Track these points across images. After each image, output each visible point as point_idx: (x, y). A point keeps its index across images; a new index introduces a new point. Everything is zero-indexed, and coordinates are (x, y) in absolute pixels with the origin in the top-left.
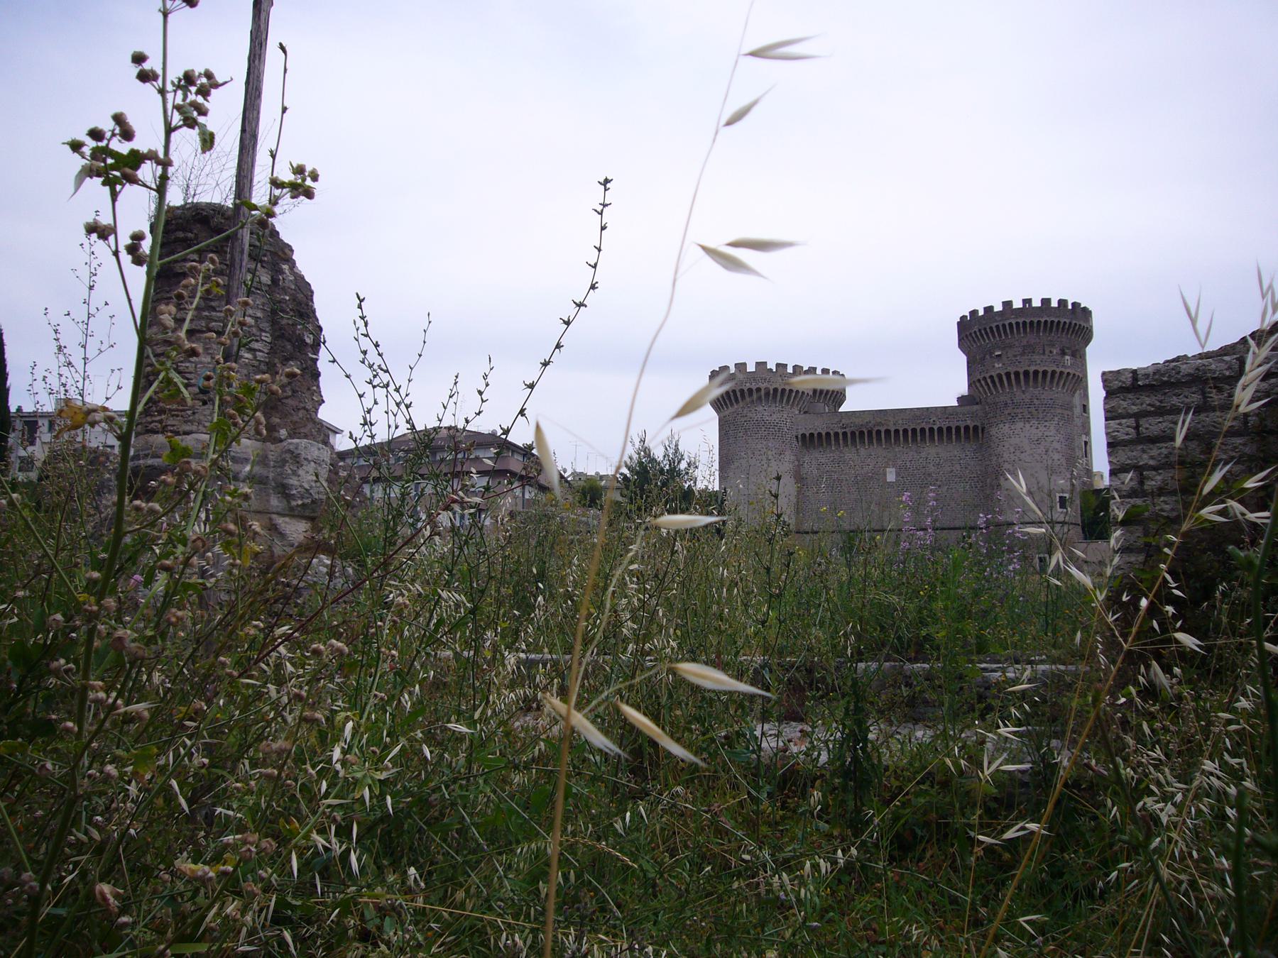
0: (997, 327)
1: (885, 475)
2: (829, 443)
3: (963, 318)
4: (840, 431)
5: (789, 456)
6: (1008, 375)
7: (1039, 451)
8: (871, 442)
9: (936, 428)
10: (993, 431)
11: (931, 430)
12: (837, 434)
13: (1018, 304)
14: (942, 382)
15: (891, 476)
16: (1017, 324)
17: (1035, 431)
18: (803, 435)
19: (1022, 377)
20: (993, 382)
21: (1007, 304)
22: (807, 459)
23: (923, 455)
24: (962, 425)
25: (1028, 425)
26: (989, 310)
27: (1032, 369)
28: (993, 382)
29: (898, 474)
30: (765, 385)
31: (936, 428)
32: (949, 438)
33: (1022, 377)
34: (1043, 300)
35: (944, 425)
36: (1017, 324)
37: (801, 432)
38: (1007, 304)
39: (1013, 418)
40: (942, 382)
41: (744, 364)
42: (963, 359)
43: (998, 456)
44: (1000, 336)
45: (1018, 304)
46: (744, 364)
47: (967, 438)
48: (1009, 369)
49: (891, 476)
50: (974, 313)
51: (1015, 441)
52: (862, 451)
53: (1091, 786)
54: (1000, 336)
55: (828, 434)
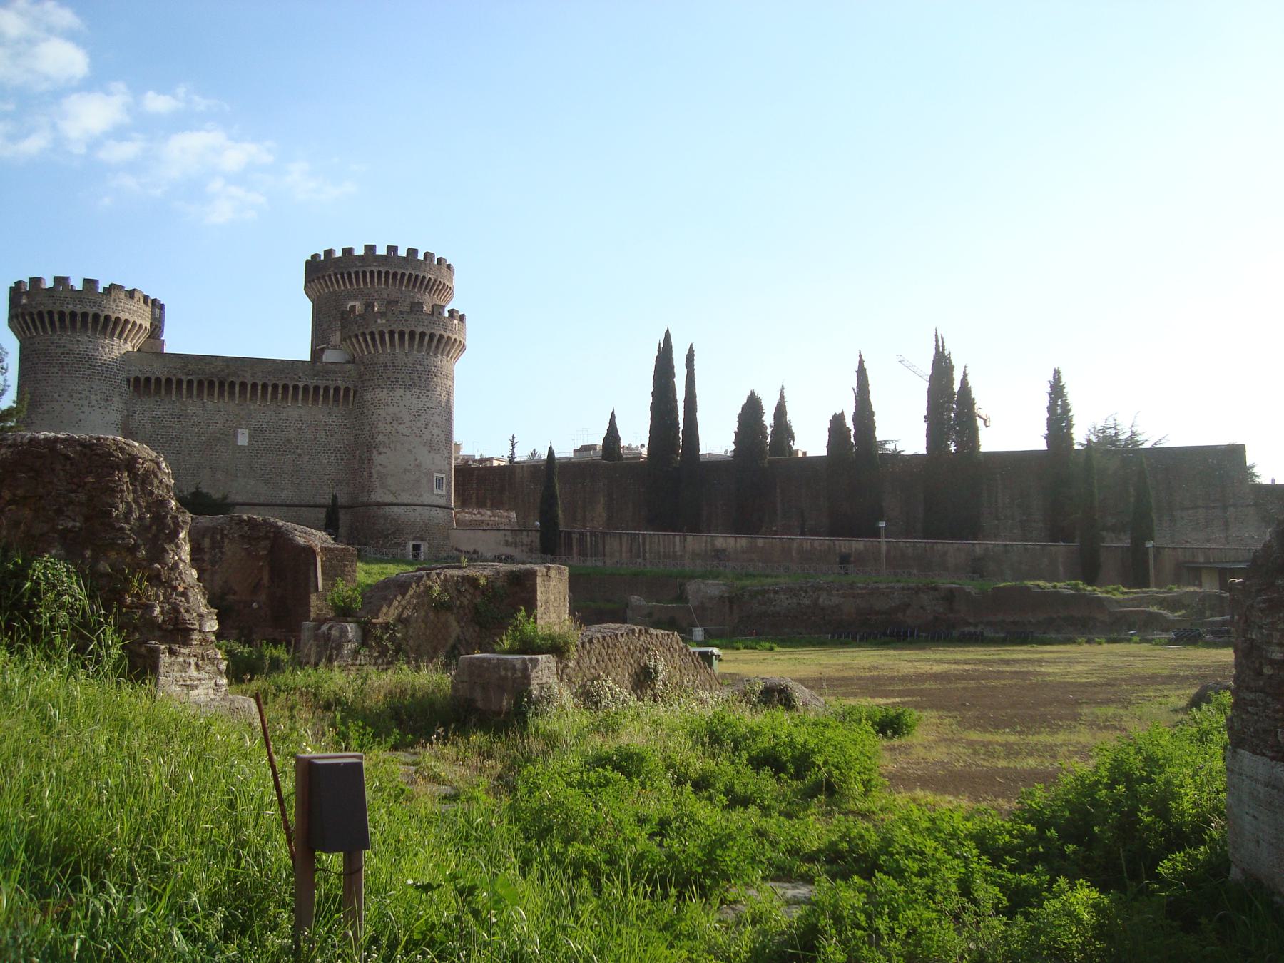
0: (403, 275)
1: (235, 436)
2: (168, 391)
3: (315, 256)
4: (185, 378)
5: (117, 403)
6: (392, 333)
7: (419, 424)
8: (316, 400)
9: (301, 385)
10: (368, 396)
11: (296, 388)
12: (180, 382)
13: (381, 251)
14: (282, 330)
15: (243, 439)
16: (410, 275)
17: (415, 400)
18: (137, 379)
19: (407, 337)
20: (373, 339)
21: (370, 249)
22: (138, 409)
23: (283, 416)
24: (332, 385)
25: (408, 393)
26: (348, 251)
27: (419, 330)
28: (373, 339)
29: (251, 437)
30: (95, 310)
31: (301, 385)
32: (316, 400)
33: (407, 337)
34: (409, 250)
35: (312, 383)
36: (380, 273)
37: (133, 375)
38: (370, 249)
39: (392, 384)
40: (282, 330)
41: (374, 247)
42: (308, 306)
43: (373, 425)
44: (358, 284)
45: (381, 251)
46: (374, 247)
47: (336, 400)
48: (394, 327)
49: (243, 439)
50: (36, 282)
51: (391, 409)
52: (210, 405)
53: (843, 943)
54: (358, 284)
55: (169, 381)
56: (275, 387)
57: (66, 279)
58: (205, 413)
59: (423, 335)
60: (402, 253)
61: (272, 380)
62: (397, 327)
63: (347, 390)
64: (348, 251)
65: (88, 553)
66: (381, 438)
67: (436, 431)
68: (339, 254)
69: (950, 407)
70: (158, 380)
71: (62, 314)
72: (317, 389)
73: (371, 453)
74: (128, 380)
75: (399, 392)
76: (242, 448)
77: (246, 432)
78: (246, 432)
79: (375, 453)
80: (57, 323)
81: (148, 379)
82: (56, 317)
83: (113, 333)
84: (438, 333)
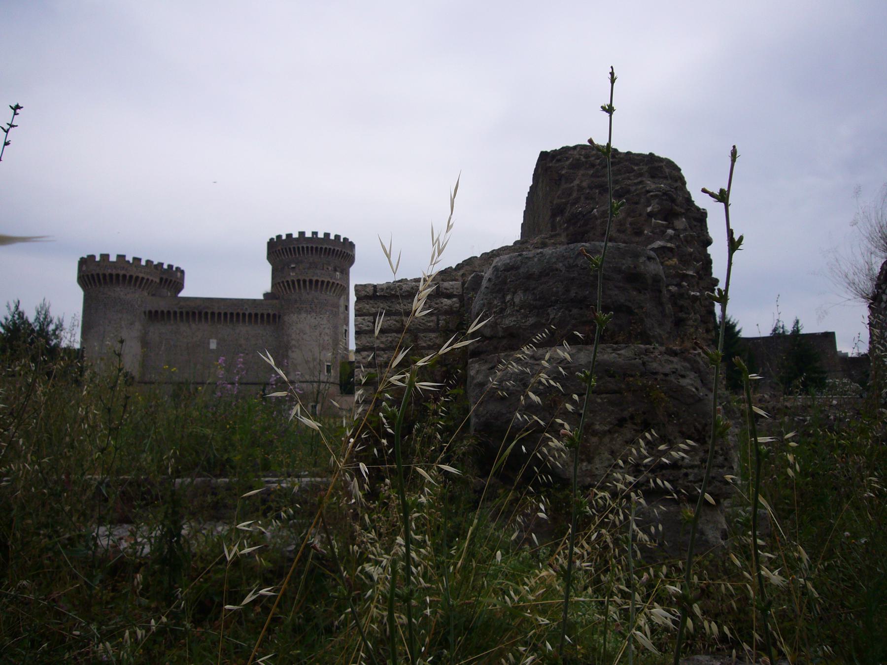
1: (209, 344)
3: (272, 239)
5: (138, 326)
6: (299, 281)
8: (256, 322)
9: (247, 313)
10: (286, 318)
13: (308, 235)
14: (254, 282)
17: (313, 320)
18: (150, 312)
19: (308, 283)
20: (288, 285)
21: (302, 234)
27: (314, 279)
28: (288, 285)
29: (218, 344)
31: (247, 313)
35: (253, 312)
37: (148, 309)
38: (302, 234)
40: (254, 282)
45: (308, 235)
49: (213, 345)
52: (194, 326)
55: (169, 312)
56: (232, 314)
57: (124, 256)
58: (190, 332)
59: (317, 281)
60: (332, 237)
61: (229, 311)
62: (301, 278)
63: (274, 315)
64: (289, 236)
65: (750, 533)
66: (293, 342)
67: (326, 338)
68: (284, 237)
69: (739, 331)
70: (162, 312)
71: (104, 275)
72: (256, 315)
73: (287, 351)
74: (145, 313)
75: (304, 315)
76: (212, 351)
77: (215, 341)
78: (215, 341)
79: (290, 352)
80: (102, 281)
81: (156, 312)
82: (101, 277)
83: (135, 285)
84: (326, 280)
